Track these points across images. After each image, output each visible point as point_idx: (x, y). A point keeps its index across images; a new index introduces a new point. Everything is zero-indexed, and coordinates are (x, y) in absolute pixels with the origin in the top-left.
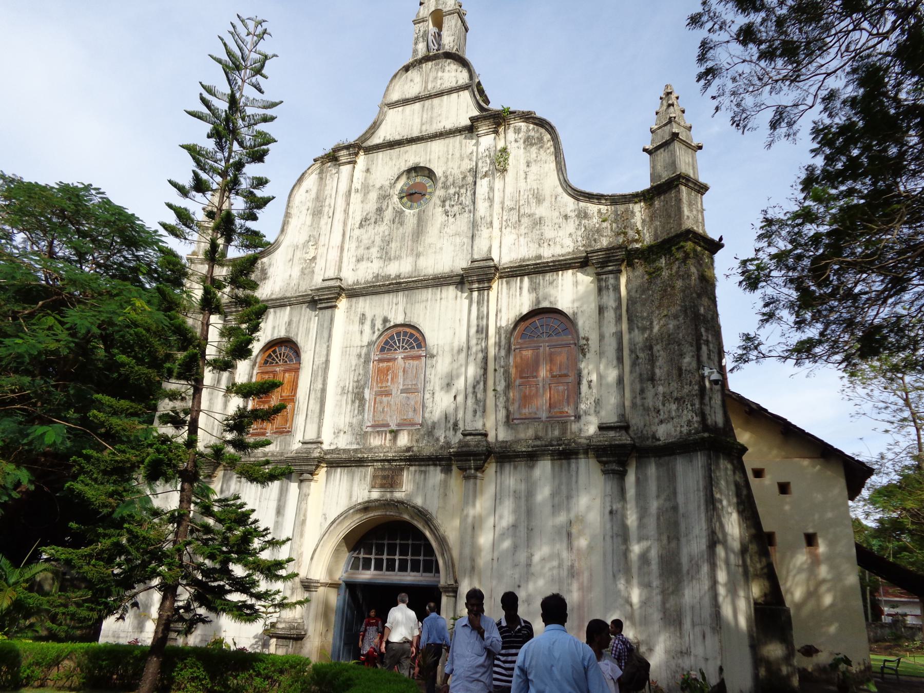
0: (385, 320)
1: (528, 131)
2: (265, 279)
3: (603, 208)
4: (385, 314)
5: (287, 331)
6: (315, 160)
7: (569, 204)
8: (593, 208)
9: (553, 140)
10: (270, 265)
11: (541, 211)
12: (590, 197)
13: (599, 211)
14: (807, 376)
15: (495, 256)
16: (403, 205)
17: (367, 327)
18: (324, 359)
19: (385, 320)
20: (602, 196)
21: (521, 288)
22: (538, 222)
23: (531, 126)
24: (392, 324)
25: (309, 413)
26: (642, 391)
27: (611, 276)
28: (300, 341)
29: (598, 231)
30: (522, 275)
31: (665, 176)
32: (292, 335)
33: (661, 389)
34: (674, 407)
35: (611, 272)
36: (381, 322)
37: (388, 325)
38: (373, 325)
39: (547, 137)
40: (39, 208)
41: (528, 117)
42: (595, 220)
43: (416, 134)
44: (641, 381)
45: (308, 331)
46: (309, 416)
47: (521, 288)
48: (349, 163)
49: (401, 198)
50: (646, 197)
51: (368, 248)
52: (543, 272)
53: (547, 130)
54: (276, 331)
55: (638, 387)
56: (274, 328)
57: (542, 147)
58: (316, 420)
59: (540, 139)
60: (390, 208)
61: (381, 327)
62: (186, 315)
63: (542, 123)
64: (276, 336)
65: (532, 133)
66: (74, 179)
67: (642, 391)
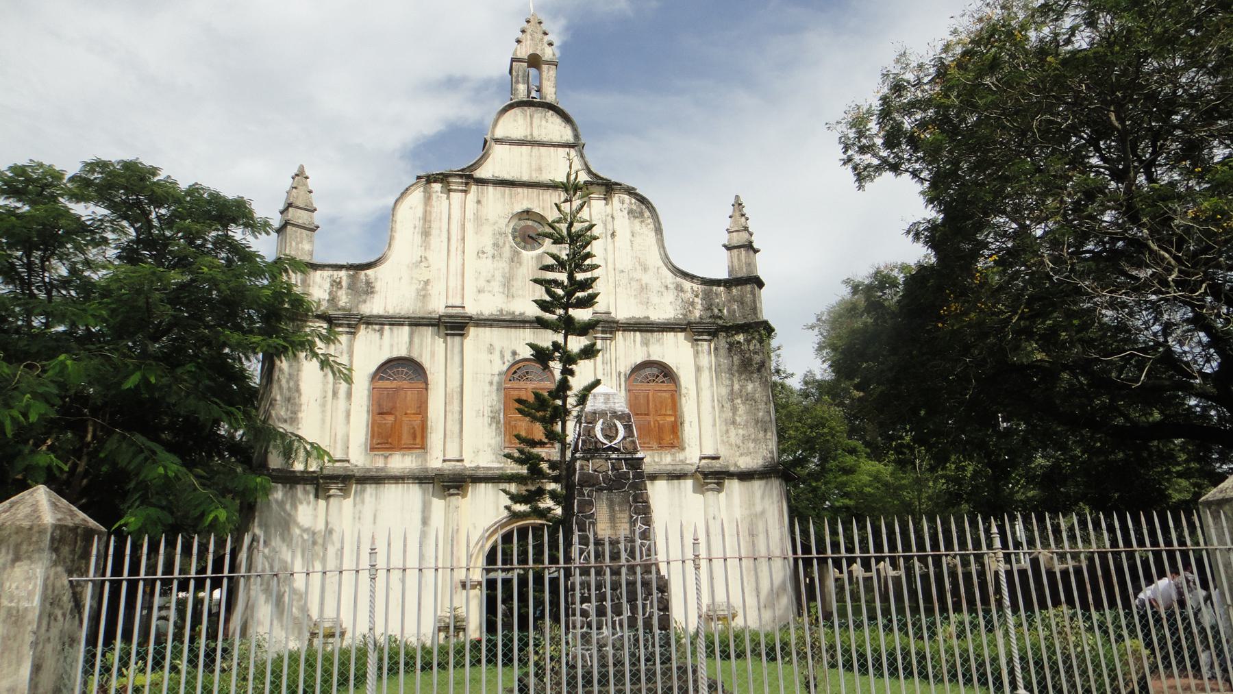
0: (514, 353)
1: (631, 203)
2: (372, 293)
3: (695, 287)
4: (513, 348)
5: (409, 350)
6: (419, 178)
7: (669, 278)
8: (687, 285)
9: (653, 218)
10: (376, 279)
11: (646, 278)
12: (685, 275)
13: (692, 288)
14: (318, 227)
15: (612, 310)
16: (518, 244)
17: (496, 357)
18: (458, 384)
19: (514, 353)
20: (696, 277)
21: (634, 341)
22: (644, 288)
23: (633, 200)
24: (521, 357)
25: (448, 432)
26: (727, 431)
27: (706, 343)
28: (426, 362)
29: (692, 304)
30: (635, 331)
31: (743, 273)
32: (415, 355)
33: (741, 432)
34: (752, 445)
35: (705, 340)
36: (510, 354)
37: (517, 358)
38: (502, 357)
39: (647, 214)
40: (1219, 309)
41: (631, 192)
42: (689, 295)
43: (525, 178)
44: (726, 424)
45: (433, 354)
46: (448, 436)
47: (634, 341)
48: (462, 191)
49: (514, 237)
50: (728, 283)
51: (488, 281)
52: (652, 331)
53: (648, 208)
54: (395, 349)
55: (724, 428)
56: (392, 346)
57: (642, 222)
58: (457, 440)
59: (642, 214)
60: (507, 245)
61: (511, 359)
62: (216, 257)
63: (642, 200)
64: (395, 354)
65: (634, 207)
66: (128, 157)
67: (727, 431)
